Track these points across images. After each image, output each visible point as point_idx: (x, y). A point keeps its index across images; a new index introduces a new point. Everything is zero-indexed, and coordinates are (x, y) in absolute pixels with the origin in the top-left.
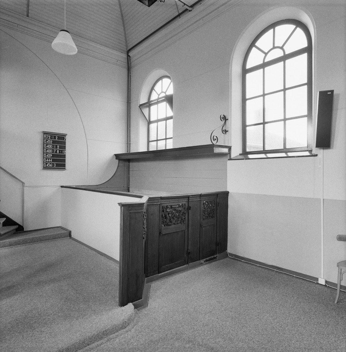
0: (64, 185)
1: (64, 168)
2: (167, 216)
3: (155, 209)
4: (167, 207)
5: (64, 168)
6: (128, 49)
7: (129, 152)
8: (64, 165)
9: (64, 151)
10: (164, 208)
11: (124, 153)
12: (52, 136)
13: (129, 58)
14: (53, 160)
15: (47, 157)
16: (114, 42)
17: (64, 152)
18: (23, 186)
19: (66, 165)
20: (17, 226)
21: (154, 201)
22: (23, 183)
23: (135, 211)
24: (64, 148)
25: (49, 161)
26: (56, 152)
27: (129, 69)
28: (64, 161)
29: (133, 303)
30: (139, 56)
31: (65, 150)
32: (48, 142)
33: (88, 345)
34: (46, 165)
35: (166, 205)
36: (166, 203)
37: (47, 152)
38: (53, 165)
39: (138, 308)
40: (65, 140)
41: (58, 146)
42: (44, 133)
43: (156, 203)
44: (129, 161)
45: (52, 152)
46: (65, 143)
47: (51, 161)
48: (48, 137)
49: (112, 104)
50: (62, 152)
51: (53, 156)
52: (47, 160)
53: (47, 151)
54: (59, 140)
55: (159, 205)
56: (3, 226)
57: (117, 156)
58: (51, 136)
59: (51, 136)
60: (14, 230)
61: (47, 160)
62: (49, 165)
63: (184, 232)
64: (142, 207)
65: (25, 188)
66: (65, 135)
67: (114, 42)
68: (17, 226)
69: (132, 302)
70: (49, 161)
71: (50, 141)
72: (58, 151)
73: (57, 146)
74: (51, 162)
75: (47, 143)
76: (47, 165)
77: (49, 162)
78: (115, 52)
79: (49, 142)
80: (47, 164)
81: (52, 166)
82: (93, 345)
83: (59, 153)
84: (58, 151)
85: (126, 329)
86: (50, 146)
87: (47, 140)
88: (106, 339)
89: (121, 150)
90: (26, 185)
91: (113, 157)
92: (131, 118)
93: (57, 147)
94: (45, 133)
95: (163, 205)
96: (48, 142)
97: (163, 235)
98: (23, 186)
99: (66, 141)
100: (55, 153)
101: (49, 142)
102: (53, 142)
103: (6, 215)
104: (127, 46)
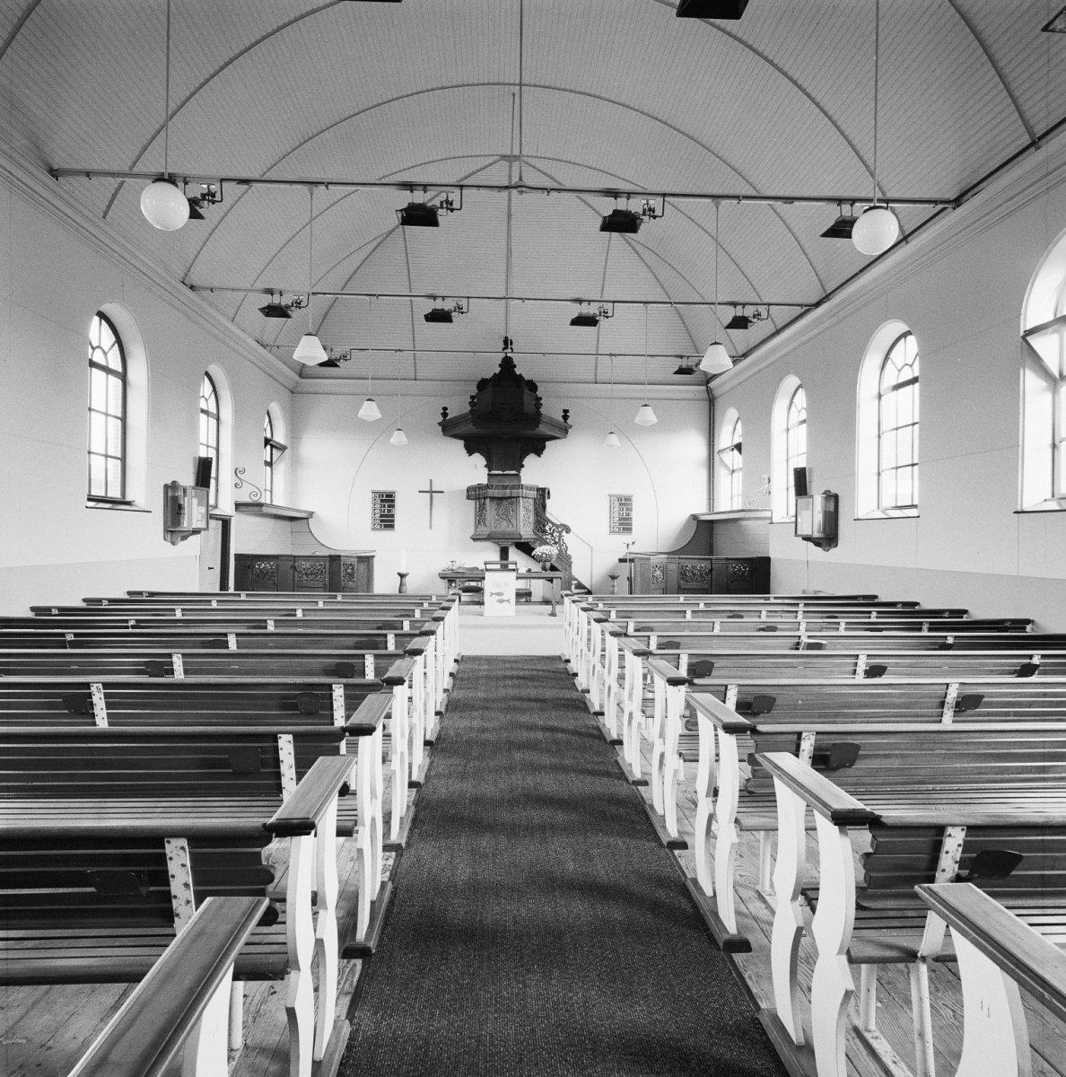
8: (392, 526)
14: (620, 524)
49: (692, 444)
71: (617, 504)
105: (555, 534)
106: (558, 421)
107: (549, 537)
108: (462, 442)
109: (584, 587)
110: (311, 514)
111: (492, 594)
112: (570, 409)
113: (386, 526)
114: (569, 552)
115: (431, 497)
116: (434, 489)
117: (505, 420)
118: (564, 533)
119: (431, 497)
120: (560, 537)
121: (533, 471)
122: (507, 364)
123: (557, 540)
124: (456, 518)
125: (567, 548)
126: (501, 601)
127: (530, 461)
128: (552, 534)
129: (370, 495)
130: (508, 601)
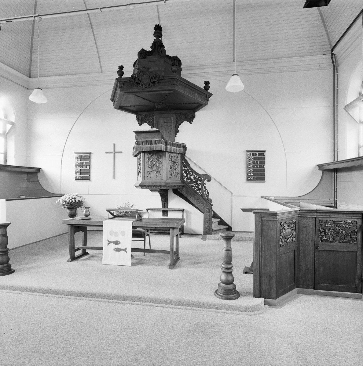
0: (264, 195)
1: (264, 181)
2: (326, 231)
3: (309, 222)
4: (326, 222)
5: (264, 181)
6: (332, 47)
7: (336, 160)
8: (264, 178)
9: (264, 165)
10: (322, 222)
11: (329, 162)
12: (253, 153)
13: (333, 56)
14: (255, 174)
15: (249, 171)
16: (315, 47)
17: (264, 167)
18: (232, 196)
19: (266, 178)
20: (228, 226)
21: (306, 214)
22: (232, 193)
23: (267, 219)
24: (264, 162)
25: (251, 174)
26: (257, 167)
27: (335, 67)
28: (264, 174)
29: (265, 299)
30: (344, 50)
31: (264, 164)
32: (250, 159)
33: (217, 309)
34: (249, 178)
35: (325, 219)
36: (321, 217)
37: (249, 167)
38: (254, 178)
39: (270, 306)
40: (265, 155)
41: (259, 162)
42: (247, 152)
43: (309, 216)
44: (336, 171)
45: (254, 167)
46: (264, 158)
47: (253, 174)
48: (250, 155)
49: (316, 110)
50: (262, 166)
51: (255, 170)
52: (250, 174)
53: (249, 166)
54: (260, 156)
55: (314, 219)
56: (218, 225)
57: (320, 167)
58: (252, 153)
59: (252, 153)
60: (225, 229)
61: (250, 174)
62: (251, 178)
63: (355, 254)
64: (275, 216)
65: (233, 198)
66: (265, 151)
67: (315, 47)
68: (228, 226)
69: (265, 298)
70: (251, 174)
71: (252, 158)
72: (258, 166)
73: (258, 161)
74: (252, 175)
75: (249, 160)
76: (250, 178)
77: (251, 175)
78: (318, 57)
79: (251, 159)
80: (249, 177)
81: (254, 179)
82: (220, 310)
83: (260, 167)
84: (258, 166)
85: (249, 313)
86: (252, 162)
87: (249, 158)
88: (230, 312)
89: (326, 159)
90: (234, 195)
91: (315, 168)
92: (339, 122)
93: (257, 163)
94: (248, 152)
95: (320, 219)
96: (250, 159)
97: (319, 250)
98: (232, 196)
99: (266, 156)
100: (256, 167)
101: (251, 159)
102: (255, 158)
103: (220, 217)
104: (330, 45)
105: (199, 182)
106: (202, 89)
107: (194, 184)
108: (135, 116)
109: (225, 224)
110: (38, 170)
111: (109, 242)
112: (267, 150)
113: (258, 178)
114: (210, 197)
115: (111, 153)
116: (117, 150)
117: (160, 93)
118: (206, 182)
119: (111, 153)
120: (203, 184)
121: (186, 134)
122: (158, 46)
123: (200, 187)
124: (130, 167)
125: (208, 193)
126: (118, 250)
127: (184, 126)
128: (196, 182)
129: (75, 156)
130: (125, 250)
